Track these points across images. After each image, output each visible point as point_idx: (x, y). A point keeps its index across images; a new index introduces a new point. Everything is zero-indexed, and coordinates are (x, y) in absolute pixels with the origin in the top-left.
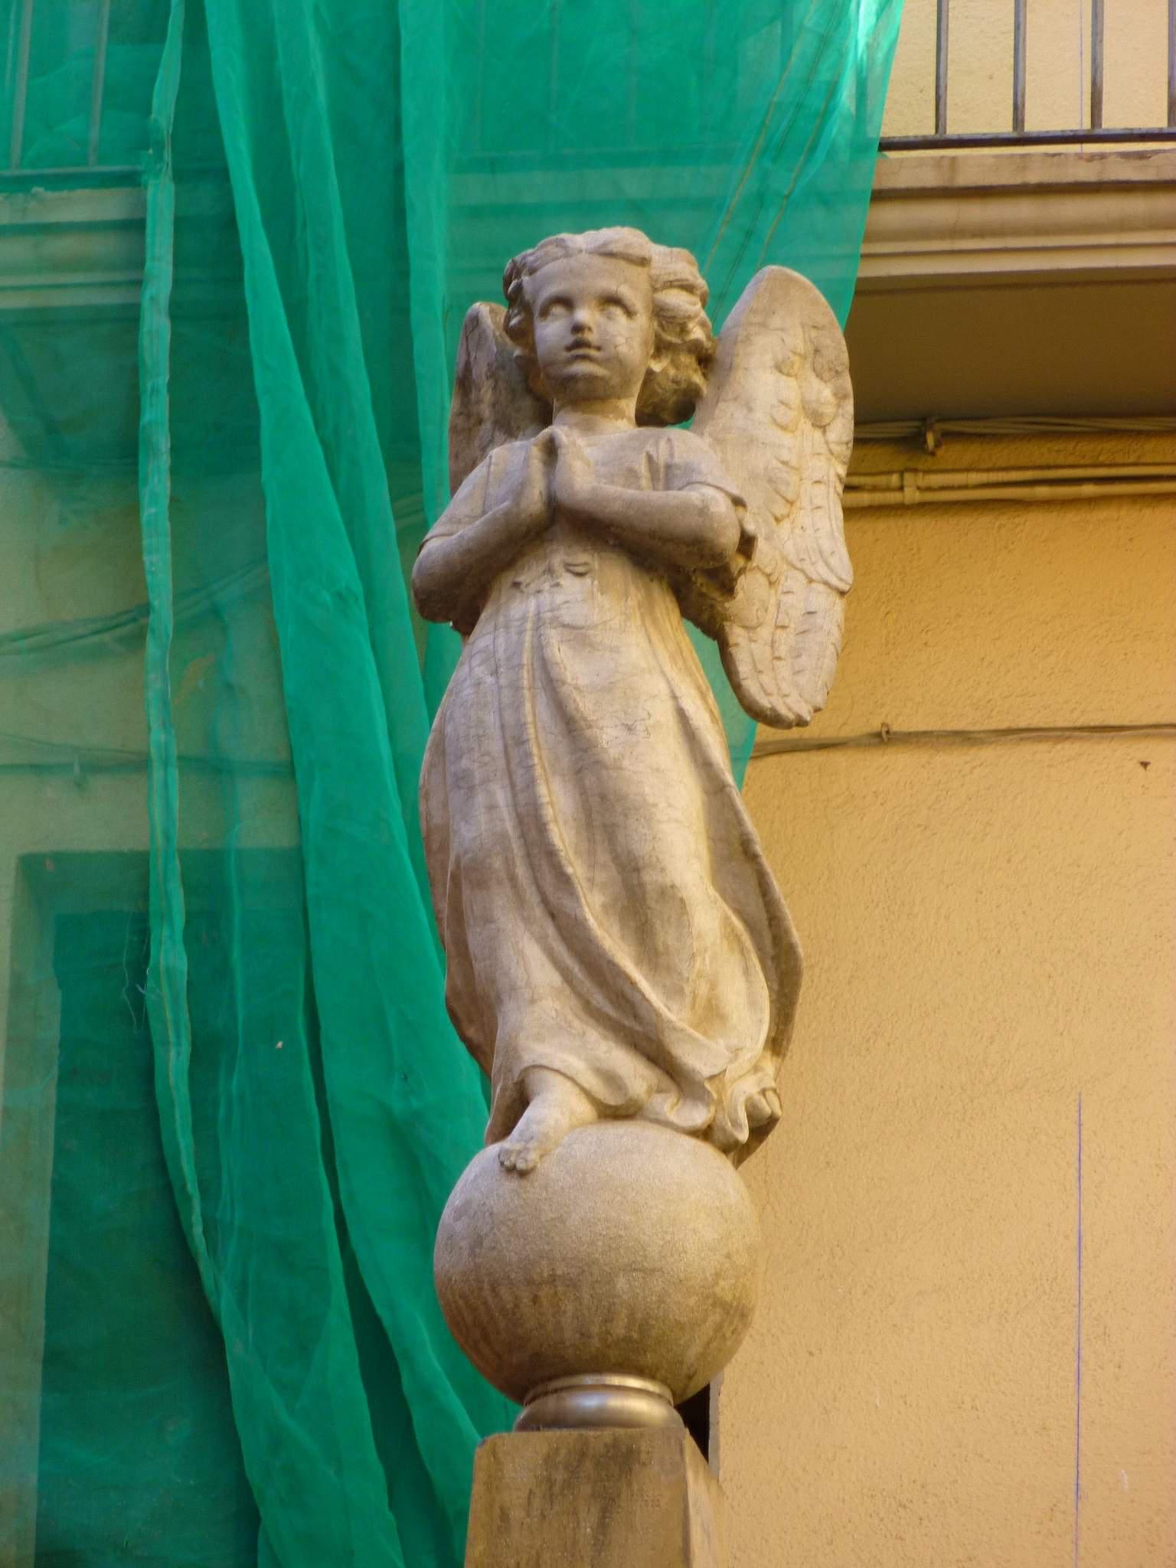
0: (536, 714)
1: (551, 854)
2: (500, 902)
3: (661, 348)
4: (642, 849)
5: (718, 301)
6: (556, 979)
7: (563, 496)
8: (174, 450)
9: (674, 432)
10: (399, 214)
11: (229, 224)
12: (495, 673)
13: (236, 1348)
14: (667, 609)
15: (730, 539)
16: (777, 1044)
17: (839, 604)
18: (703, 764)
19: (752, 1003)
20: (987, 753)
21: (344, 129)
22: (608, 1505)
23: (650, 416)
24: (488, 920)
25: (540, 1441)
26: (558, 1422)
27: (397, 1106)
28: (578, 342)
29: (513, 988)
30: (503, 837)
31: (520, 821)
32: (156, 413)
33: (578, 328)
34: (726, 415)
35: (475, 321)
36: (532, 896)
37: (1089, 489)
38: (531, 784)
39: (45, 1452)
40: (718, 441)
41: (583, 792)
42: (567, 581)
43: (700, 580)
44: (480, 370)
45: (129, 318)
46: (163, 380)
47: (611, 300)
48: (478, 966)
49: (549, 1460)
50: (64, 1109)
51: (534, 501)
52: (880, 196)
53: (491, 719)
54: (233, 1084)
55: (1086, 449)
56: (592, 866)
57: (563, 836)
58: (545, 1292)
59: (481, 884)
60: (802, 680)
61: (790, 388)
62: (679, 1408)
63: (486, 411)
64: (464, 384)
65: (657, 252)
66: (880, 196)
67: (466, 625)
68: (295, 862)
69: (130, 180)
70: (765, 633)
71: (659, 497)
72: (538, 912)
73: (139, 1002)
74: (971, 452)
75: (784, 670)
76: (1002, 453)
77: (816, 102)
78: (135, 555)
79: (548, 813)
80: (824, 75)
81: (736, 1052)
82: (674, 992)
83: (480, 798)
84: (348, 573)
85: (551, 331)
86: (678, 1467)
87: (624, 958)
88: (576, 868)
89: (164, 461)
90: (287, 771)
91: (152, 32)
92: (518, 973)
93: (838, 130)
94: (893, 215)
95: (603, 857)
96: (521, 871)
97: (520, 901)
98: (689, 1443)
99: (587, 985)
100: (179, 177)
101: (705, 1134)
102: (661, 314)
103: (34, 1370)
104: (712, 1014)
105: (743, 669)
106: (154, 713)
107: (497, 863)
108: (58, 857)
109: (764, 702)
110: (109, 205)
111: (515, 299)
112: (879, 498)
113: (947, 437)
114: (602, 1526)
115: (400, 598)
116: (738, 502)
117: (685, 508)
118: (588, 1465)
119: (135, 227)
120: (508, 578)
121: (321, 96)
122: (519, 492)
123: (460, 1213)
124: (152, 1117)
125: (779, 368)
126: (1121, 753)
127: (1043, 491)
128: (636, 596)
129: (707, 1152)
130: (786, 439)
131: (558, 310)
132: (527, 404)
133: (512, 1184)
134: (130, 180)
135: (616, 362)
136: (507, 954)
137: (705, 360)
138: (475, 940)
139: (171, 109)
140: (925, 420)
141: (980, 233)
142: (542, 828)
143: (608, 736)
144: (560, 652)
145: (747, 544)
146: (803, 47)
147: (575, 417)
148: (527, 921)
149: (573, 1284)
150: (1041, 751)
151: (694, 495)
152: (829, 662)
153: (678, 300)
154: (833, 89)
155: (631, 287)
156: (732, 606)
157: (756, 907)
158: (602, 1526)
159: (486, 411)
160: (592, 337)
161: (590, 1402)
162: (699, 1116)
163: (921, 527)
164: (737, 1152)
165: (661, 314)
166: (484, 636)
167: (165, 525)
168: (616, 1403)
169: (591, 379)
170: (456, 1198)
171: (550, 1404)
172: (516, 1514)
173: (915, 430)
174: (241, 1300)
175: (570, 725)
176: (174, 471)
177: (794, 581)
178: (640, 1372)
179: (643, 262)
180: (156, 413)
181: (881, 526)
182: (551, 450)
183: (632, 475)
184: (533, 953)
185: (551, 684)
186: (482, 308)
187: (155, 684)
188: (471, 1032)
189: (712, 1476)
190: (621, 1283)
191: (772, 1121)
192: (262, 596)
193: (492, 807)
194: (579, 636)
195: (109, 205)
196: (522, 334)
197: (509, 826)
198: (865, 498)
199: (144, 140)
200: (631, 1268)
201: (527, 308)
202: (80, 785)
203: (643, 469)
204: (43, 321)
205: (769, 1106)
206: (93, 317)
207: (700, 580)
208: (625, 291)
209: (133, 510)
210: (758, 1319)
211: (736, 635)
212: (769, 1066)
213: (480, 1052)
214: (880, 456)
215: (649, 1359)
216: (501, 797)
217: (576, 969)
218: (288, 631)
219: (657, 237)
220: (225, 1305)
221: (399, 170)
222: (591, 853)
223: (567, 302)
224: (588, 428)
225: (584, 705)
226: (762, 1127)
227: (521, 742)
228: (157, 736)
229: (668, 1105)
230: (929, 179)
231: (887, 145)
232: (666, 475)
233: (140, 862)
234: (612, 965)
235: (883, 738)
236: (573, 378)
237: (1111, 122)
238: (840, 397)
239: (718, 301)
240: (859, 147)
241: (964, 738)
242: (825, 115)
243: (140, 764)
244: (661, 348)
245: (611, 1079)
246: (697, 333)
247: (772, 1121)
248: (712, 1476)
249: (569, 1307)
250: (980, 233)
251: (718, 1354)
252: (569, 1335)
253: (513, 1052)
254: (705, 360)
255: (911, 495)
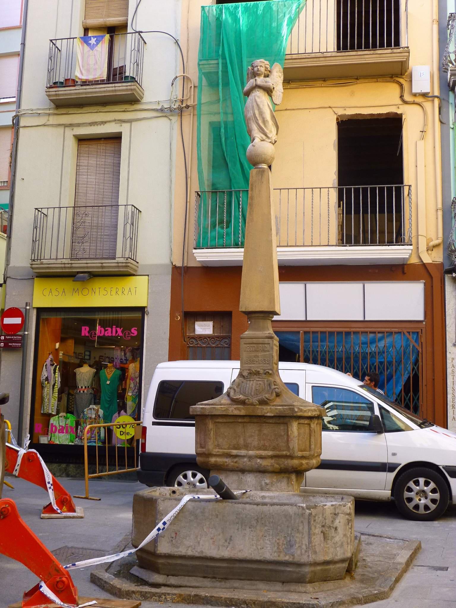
0: (255, 104)
1: (256, 117)
2: (252, 123)
3: (266, 70)
4: (264, 117)
5: (271, 66)
6: (257, 128)
7: (257, 84)
8: (222, 84)
9: (267, 78)
10: (242, 62)
11: (226, 63)
12: (251, 100)
13: (229, 165)
14: (267, 94)
15: (272, 88)
16: (277, 134)
17: (282, 94)
18: (270, 109)
19: (274, 130)
20: (296, 111)
21: (237, 55)
22: (262, 175)
23: (265, 77)
24: (250, 123)
25: (256, 170)
26: (257, 168)
27: (243, 144)
28: (258, 70)
29: (253, 130)
30: (252, 115)
31: (253, 114)
32: (220, 81)
33: (258, 69)
34: (272, 76)
35: (249, 68)
36: (254, 121)
37: (304, 87)
38: (254, 110)
39: (213, 175)
40: (271, 79)
41: (259, 111)
42: (257, 92)
43: (269, 92)
44: (249, 73)
45: (218, 72)
46: (221, 77)
47: (261, 66)
48: (250, 127)
49: (257, 172)
50: (213, 144)
51: (254, 84)
52: (286, 59)
53: (251, 105)
54: (228, 142)
55: (304, 83)
56: (260, 118)
57: (257, 115)
58: (256, 157)
59: (250, 120)
60: (279, 101)
61: (277, 74)
62: (268, 167)
63: (250, 77)
64: (248, 74)
65: (265, 62)
66: (286, 59)
67: (248, 96)
68: (233, 122)
69: (217, 59)
70: (275, 96)
71: (266, 84)
72: (255, 122)
73: (220, 135)
74: (294, 83)
75: (277, 100)
76: (297, 83)
77: (280, 51)
78: (219, 94)
79: (256, 113)
80: (280, 48)
81: (273, 135)
82: (268, 129)
83: (250, 112)
84: (238, 95)
85: (256, 69)
86: (268, 172)
87: (263, 127)
88: (258, 118)
89: (221, 85)
90: (233, 114)
91: (219, 45)
92: (253, 128)
93: (282, 53)
94: (287, 61)
95: (261, 117)
96: (254, 119)
97: (253, 121)
98: (269, 170)
99: (260, 129)
100: (222, 59)
101: (270, 142)
102: (265, 67)
103: (212, 168)
104: (271, 132)
105: (273, 100)
106: (221, 109)
107: (251, 118)
108: (212, 122)
109: (275, 103)
110: (216, 62)
111: (252, 66)
112: (286, 88)
113: (291, 82)
114: (262, 177)
115: (242, 95)
116: (273, 84)
117: (268, 85)
118: (260, 172)
119: (218, 64)
120: (252, 92)
121: (235, 51)
122: (253, 84)
123: (248, 150)
124: (221, 145)
125: (276, 72)
126: (308, 110)
127: (300, 87)
128: (264, 93)
129: (271, 144)
130: (277, 79)
131: (256, 67)
132: (253, 76)
133: (253, 147)
134: (217, 59)
135: (262, 72)
136: (252, 126)
137: (270, 72)
138: (249, 125)
139: (221, 53)
140: (290, 80)
141: (295, 63)
142: (255, 115)
143: (261, 106)
144: (257, 98)
145: (274, 88)
146: (278, 46)
147: (258, 77)
148: (254, 123)
149: (259, 156)
150: (300, 111)
151: (269, 84)
152: (281, 99)
153: (267, 66)
154: (281, 49)
155: (263, 65)
156: (272, 94)
157: (275, 122)
158: (262, 177)
159: (250, 77)
160: (259, 69)
161: (260, 166)
162: (270, 141)
163: (289, 90)
164: (273, 144)
165: (265, 67)
166: (250, 97)
167: (221, 91)
168: (263, 166)
169: (259, 73)
170: (248, 148)
171: (257, 166)
172: (254, 176)
173: (283, 36)
174: (230, 161)
175: (258, 105)
176: (222, 86)
177: (278, 92)
178: (265, 164)
179: (264, 62)
180: (220, 81)
181: (286, 90)
182: (256, 80)
183: (263, 82)
184: (255, 126)
185: (256, 102)
186: (249, 67)
187: (221, 105)
188: (250, 134)
189: (271, 173)
190: (263, 156)
191: (276, 141)
192: (230, 98)
193: (251, 113)
194: (259, 97)
195: (216, 62)
196: (253, 69)
197: (252, 114)
198: (285, 88)
199: (219, 55)
200: (264, 154)
201: (253, 67)
202: (214, 115)
203: (264, 81)
204: (210, 73)
205: (276, 140)
206: (214, 72)
207: (269, 92)
208: (262, 65)
209: (218, 90)
210: (275, 158)
211: (273, 97)
212: (276, 136)
213: (250, 135)
214: (286, 84)
215: (266, 162)
216: (252, 112)
217: (259, 128)
218: (232, 100)
219: (265, 60)
220: (228, 161)
221: (242, 58)
222: (260, 117)
223: (257, 66)
224: (259, 78)
225: (259, 103)
226: (275, 142)
227: (253, 107)
228: (221, 110)
229: (267, 140)
230: (290, 58)
231: (286, 55)
232: (266, 82)
233: (220, 122)
234: (262, 127)
235: (286, 110)
236: (257, 73)
237: (307, 52)
238: (282, 75)
239: (271, 66)
240: (284, 55)
241: (293, 110)
242: (280, 52)
243: (220, 113)
244: (266, 70)
245: (262, 137)
246: (269, 69)
247: (276, 141)
248: (271, 173)
249: (258, 158)
250: (295, 63)
251: (272, 161)
252: (258, 160)
253: (253, 135)
254: (270, 72)
255: (289, 87)
